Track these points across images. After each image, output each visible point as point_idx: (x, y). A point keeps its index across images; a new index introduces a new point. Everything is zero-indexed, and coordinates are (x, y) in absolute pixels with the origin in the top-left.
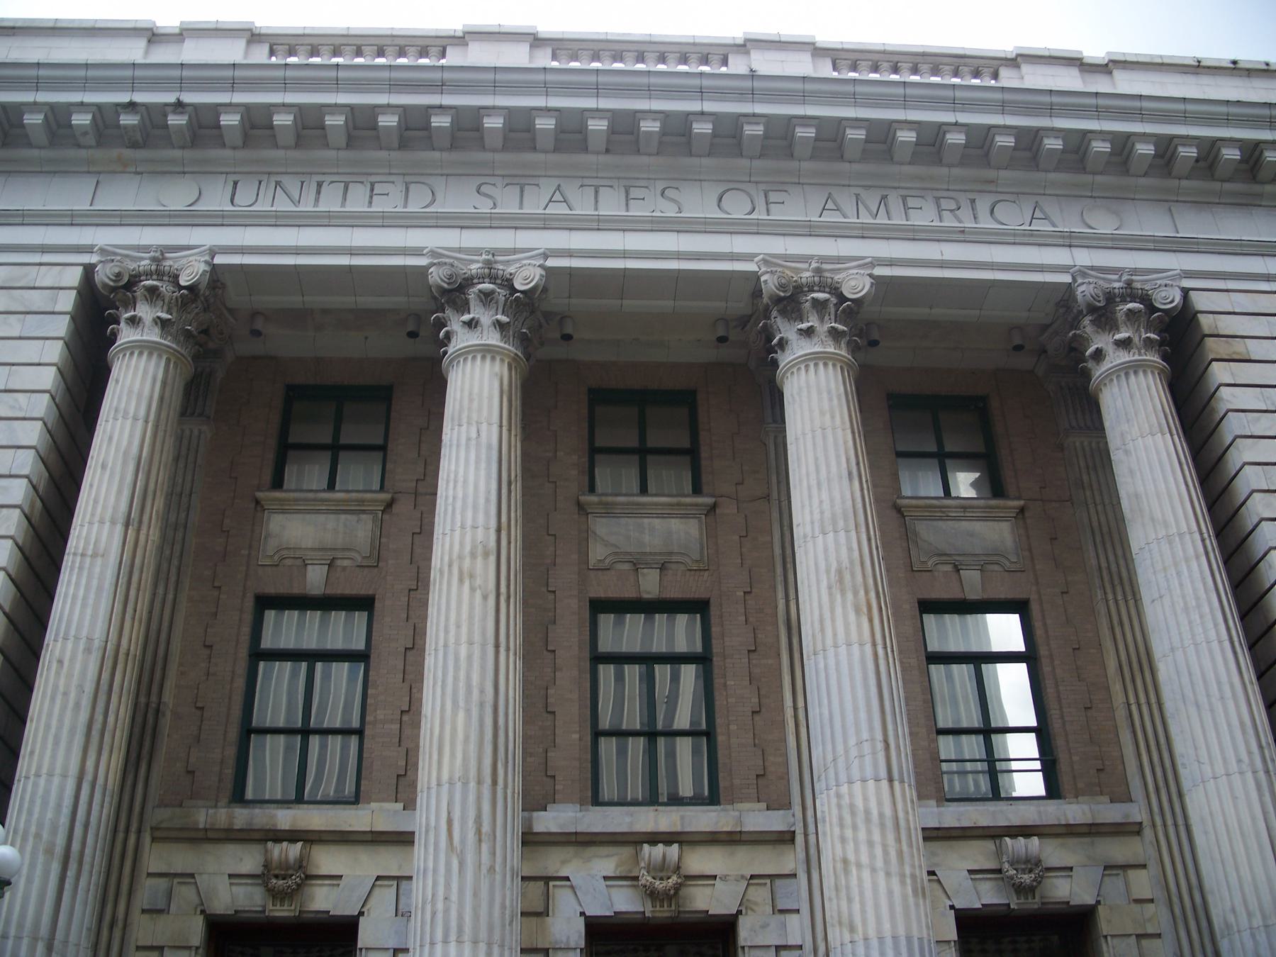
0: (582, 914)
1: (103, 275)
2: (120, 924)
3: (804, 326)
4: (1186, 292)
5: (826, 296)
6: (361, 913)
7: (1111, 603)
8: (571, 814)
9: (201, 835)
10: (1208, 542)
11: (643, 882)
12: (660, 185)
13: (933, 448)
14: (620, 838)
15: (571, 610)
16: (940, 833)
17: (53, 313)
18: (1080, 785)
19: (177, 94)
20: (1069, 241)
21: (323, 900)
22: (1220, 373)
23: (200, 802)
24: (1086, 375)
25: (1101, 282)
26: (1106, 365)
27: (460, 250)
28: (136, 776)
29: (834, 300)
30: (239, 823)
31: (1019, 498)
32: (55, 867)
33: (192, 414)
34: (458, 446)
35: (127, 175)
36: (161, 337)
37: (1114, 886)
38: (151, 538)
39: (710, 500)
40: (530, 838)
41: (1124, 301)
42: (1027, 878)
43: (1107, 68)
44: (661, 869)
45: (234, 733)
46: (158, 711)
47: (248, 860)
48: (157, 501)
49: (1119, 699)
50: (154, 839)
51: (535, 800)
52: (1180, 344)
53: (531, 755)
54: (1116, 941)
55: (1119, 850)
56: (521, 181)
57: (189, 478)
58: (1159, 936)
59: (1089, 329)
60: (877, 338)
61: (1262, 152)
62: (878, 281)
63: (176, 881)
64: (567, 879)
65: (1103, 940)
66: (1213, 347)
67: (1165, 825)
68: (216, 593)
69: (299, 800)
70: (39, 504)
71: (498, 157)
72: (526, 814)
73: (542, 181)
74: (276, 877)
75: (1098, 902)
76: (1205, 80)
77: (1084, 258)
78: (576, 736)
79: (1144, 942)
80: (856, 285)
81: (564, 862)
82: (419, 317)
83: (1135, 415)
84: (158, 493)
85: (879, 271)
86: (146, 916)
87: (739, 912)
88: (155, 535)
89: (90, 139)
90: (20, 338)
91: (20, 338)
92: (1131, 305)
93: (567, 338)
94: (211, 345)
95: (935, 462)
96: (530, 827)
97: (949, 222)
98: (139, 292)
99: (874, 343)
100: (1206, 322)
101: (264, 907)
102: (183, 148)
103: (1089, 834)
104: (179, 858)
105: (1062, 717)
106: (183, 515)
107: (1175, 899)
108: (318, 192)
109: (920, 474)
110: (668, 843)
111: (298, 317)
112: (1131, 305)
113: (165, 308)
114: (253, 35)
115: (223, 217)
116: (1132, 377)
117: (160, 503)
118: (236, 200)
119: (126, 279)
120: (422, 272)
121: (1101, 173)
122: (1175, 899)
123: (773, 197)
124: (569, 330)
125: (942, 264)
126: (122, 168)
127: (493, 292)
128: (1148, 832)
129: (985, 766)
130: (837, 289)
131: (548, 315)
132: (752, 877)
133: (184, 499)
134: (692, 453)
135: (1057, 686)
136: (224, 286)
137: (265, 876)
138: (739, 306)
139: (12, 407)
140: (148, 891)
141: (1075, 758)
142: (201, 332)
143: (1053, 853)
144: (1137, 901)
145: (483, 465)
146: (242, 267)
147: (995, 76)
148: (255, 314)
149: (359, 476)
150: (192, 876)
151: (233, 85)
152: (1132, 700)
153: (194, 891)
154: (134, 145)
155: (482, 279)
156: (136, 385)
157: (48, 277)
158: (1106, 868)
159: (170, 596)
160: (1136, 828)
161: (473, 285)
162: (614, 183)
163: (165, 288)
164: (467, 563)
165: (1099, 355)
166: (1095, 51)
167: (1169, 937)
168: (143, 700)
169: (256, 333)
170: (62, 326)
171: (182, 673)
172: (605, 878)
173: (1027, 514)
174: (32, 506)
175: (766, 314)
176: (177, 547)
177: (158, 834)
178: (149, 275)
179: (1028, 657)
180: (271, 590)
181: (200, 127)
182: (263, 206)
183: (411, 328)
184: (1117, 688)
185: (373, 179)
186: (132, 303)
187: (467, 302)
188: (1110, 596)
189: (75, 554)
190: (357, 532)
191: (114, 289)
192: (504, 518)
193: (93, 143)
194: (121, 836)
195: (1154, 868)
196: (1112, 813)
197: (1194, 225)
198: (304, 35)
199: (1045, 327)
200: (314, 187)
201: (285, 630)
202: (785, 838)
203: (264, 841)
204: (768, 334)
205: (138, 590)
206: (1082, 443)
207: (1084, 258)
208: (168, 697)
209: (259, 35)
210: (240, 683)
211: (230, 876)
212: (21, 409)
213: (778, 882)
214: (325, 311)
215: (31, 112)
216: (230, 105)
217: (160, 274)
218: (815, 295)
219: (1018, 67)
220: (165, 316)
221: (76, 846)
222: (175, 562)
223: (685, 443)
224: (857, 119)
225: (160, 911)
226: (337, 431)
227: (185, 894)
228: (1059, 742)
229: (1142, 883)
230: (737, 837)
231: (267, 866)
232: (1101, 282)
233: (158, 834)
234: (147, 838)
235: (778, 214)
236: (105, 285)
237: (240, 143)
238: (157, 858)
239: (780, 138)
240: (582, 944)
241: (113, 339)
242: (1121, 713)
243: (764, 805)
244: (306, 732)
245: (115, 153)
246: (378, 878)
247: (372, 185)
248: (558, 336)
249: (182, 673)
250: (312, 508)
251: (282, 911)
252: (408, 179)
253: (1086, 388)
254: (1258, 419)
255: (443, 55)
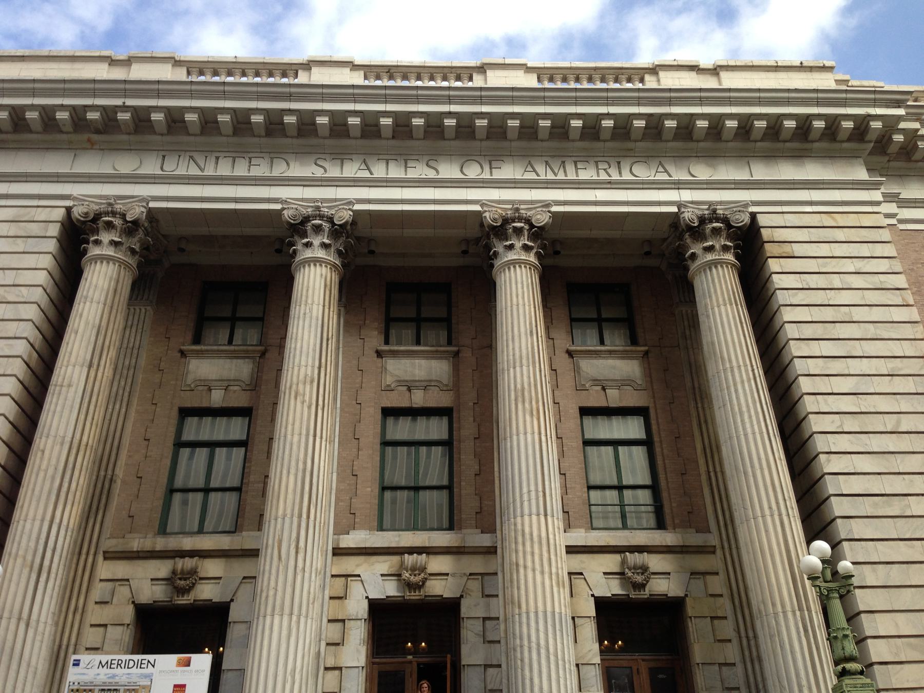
0: (367, 597)
1: (77, 212)
2: (80, 610)
3: (508, 243)
4: (753, 216)
5: (522, 225)
6: (232, 600)
7: (700, 409)
8: (363, 536)
9: (135, 555)
10: (756, 371)
11: (404, 577)
12: (426, 158)
13: (595, 316)
14: (391, 551)
15: (372, 415)
16: (586, 549)
17: (45, 237)
18: (677, 521)
19: (123, 100)
20: (678, 185)
21: (206, 592)
22: (774, 265)
23: (136, 535)
24: (687, 269)
25: (696, 211)
26: (698, 262)
27: (302, 200)
28: (95, 520)
29: (527, 227)
30: (158, 548)
31: (645, 345)
32: (34, 577)
33: (136, 299)
34: (299, 318)
35: (93, 151)
36: (115, 252)
37: (698, 584)
38: (106, 374)
39: (455, 349)
40: (336, 551)
41: (711, 221)
42: (639, 579)
43: (715, 71)
44: (414, 569)
45: (161, 491)
46: (111, 480)
47: (162, 569)
48: (110, 353)
49: (703, 469)
50: (105, 558)
51: (342, 529)
52: (748, 246)
53: (342, 501)
54: (698, 620)
55: (701, 563)
56: (341, 157)
57: (138, 338)
58: (725, 618)
59: (689, 241)
60: (559, 249)
61: (811, 122)
62: (555, 215)
63: (118, 583)
64: (359, 576)
65: (689, 620)
66: (769, 249)
67: (730, 549)
68: (154, 407)
69: (201, 531)
70: (35, 355)
71: (327, 142)
72: (336, 537)
73: (354, 157)
74: (180, 579)
75: (686, 595)
76: (782, 75)
77: (686, 195)
78: (369, 489)
79: (716, 622)
80: (542, 219)
81: (358, 566)
82: (282, 240)
83: (719, 292)
84: (112, 347)
85: (555, 209)
86: (98, 606)
87: (462, 596)
88: (109, 372)
89: (69, 128)
90: (24, 253)
91: (24, 253)
92: (715, 225)
93: (372, 252)
94: (152, 257)
95: (596, 324)
96: (338, 544)
97: (603, 176)
98: (101, 224)
99: (557, 253)
100: (766, 234)
101: (172, 598)
102: (129, 134)
103: (681, 552)
104: (120, 569)
105: (667, 479)
106: (134, 361)
107: (736, 595)
108: (217, 163)
109: (588, 331)
110: (420, 553)
111: (209, 240)
112: (715, 225)
113: (118, 234)
114: (176, 61)
115: (155, 178)
116: (714, 270)
117: (113, 353)
118: (164, 168)
119: (92, 216)
120: (279, 213)
121: (702, 141)
122: (736, 595)
123: (494, 164)
124: (373, 248)
125: (596, 203)
126: (91, 146)
127: (321, 225)
128: (719, 552)
129: (618, 508)
130: (529, 220)
131: (358, 239)
132: (471, 574)
133: (135, 351)
134: (447, 322)
135: (664, 460)
136: (157, 221)
137: (169, 581)
138: (474, 232)
139: (18, 296)
140: (99, 591)
141: (674, 505)
142: (144, 249)
143: (655, 562)
144: (712, 595)
145: (313, 329)
146: (168, 210)
147: (642, 80)
148: (181, 238)
149: (248, 335)
150: (128, 580)
151: (159, 95)
152: (711, 469)
153: (129, 590)
154: (98, 132)
155: (315, 217)
156: (101, 281)
157: (42, 215)
158: (692, 574)
159: (123, 410)
160: (712, 549)
161: (310, 221)
162: (398, 157)
163: (117, 222)
164: (301, 387)
165: (694, 256)
166: (706, 62)
167: (735, 641)
168: (102, 473)
169: (182, 250)
170: (51, 245)
171: (130, 456)
172: (382, 575)
173: (650, 355)
174: (30, 356)
175: (488, 237)
176: (129, 381)
177: (107, 555)
178: (107, 214)
179: (647, 443)
180: (188, 405)
181: (140, 121)
182: (181, 171)
183: (277, 246)
184: (702, 461)
185: (251, 155)
186: (96, 231)
187: (306, 232)
188: (700, 405)
189: (56, 385)
190: (242, 369)
191: (84, 222)
192: (323, 360)
193: (71, 130)
194: (83, 557)
195: (722, 575)
196: (695, 539)
197: (760, 172)
198: (208, 62)
199: (665, 240)
200: (214, 159)
201: (195, 429)
202: (491, 551)
203: (173, 557)
204: (488, 247)
205: (96, 406)
206: (687, 311)
207: (686, 195)
208: (119, 472)
209: (180, 61)
210: (168, 462)
211: (152, 580)
212: (23, 296)
213: (486, 578)
214: (224, 237)
215: (30, 110)
216: (157, 107)
217: (114, 214)
218: (515, 224)
219: (657, 74)
220: (117, 239)
221: (46, 563)
222: (128, 389)
223: (445, 315)
224: (545, 114)
225: (106, 603)
226: (234, 311)
227: (123, 592)
228: (665, 495)
229: (716, 584)
230: (462, 550)
231: (174, 572)
232: (696, 211)
233: (107, 555)
234: (100, 558)
235: (498, 175)
236: (78, 220)
237: (165, 132)
238: (106, 569)
239: (497, 129)
240: (366, 616)
241: (85, 252)
242: (704, 477)
243: (480, 531)
244: (207, 491)
245: (86, 136)
246: (245, 578)
247: (250, 158)
248: (366, 251)
249: (130, 456)
250: (218, 354)
251: (183, 600)
252: (272, 155)
253: (686, 276)
254: (796, 294)
255: (296, 76)
